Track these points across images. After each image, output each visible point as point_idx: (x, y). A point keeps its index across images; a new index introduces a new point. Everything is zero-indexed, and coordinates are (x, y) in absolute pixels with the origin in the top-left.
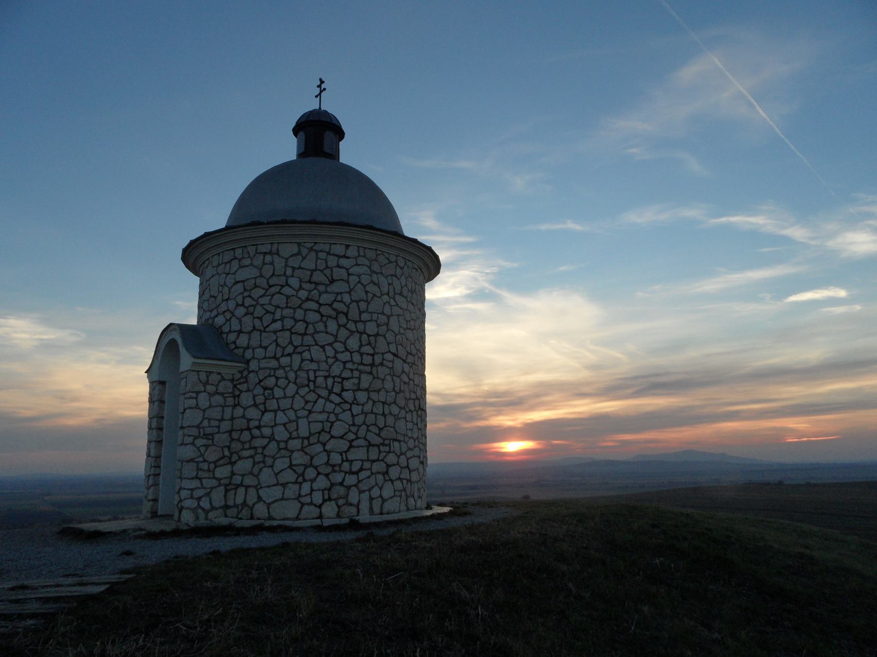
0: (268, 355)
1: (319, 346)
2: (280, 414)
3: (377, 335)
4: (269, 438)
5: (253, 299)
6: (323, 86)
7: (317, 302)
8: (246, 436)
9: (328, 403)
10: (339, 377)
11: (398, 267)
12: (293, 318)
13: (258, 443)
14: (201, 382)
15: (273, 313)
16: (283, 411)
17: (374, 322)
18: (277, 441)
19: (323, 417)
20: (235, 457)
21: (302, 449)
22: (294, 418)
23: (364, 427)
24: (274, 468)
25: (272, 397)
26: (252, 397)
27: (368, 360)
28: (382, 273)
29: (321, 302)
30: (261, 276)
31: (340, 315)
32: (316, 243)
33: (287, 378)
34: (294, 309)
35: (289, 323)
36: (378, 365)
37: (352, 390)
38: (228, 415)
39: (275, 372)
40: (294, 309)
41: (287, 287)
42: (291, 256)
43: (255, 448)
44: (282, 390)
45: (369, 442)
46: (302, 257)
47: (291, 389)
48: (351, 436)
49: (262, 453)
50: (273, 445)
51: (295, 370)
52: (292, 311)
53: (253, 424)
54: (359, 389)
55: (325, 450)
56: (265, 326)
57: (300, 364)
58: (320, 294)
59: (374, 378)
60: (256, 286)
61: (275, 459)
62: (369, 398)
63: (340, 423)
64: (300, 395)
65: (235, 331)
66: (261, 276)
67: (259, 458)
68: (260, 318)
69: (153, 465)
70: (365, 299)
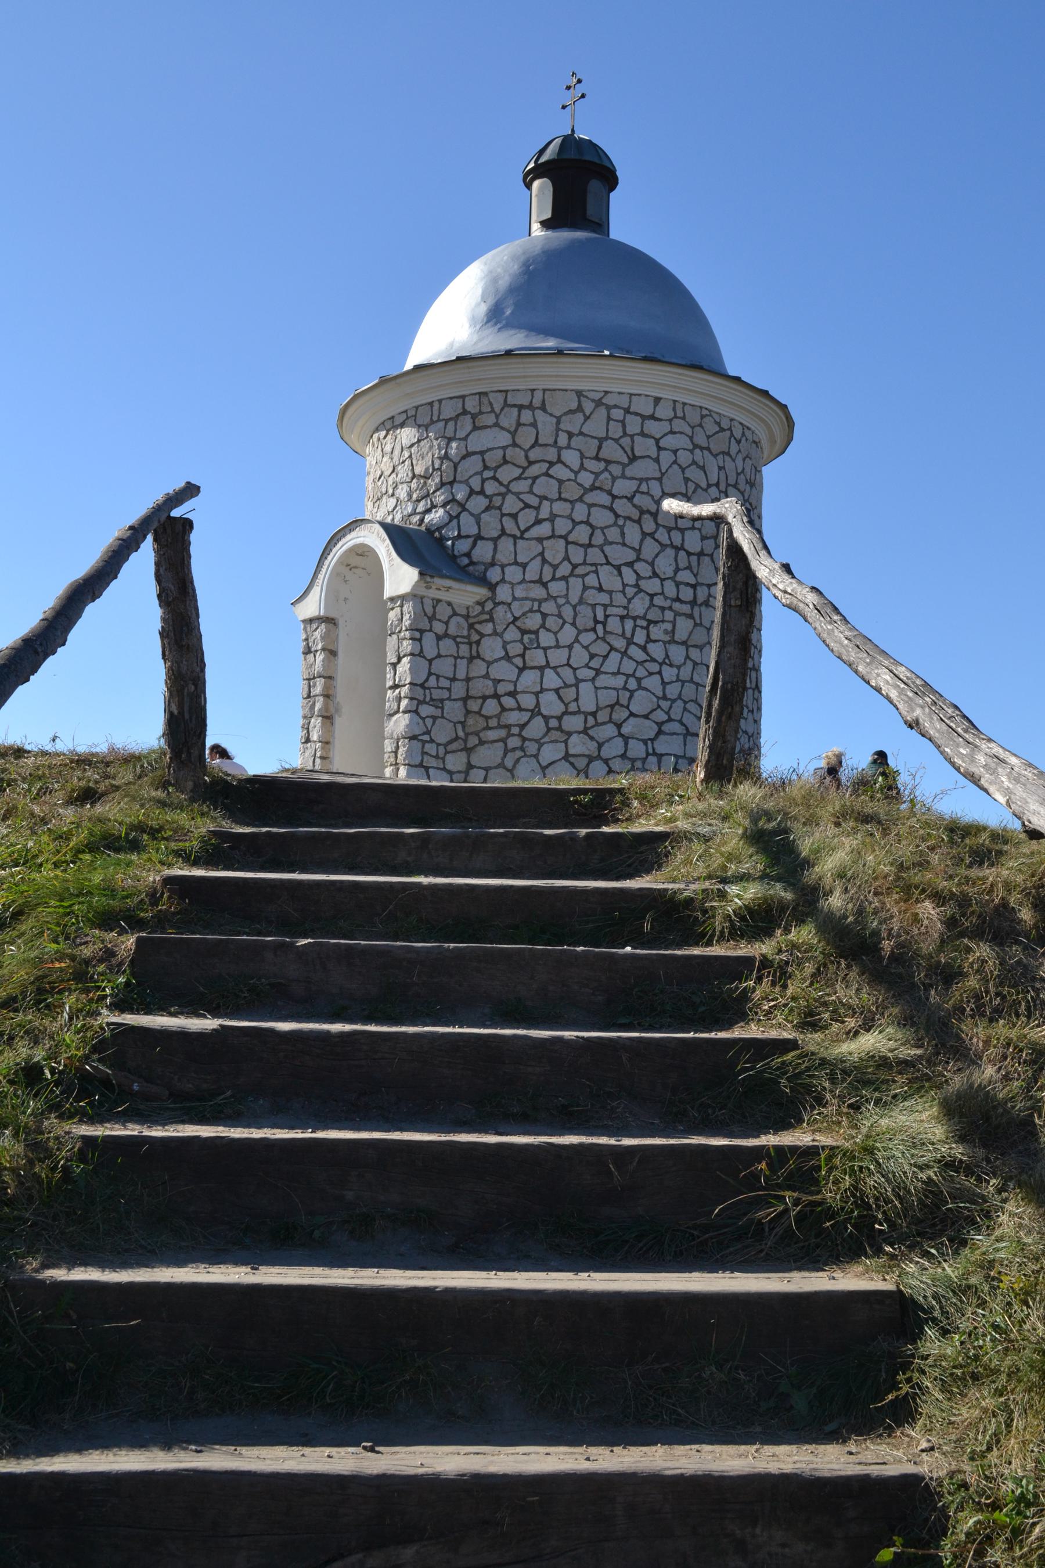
0: (527, 578)
1: (612, 565)
2: (548, 672)
3: (701, 554)
4: (532, 711)
5: (501, 484)
6: (580, 89)
7: (610, 493)
8: (491, 707)
9: (625, 658)
10: (644, 618)
11: (732, 438)
12: (570, 517)
13: (514, 718)
14: (426, 615)
15: (537, 509)
16: (555, 668)
17: (697, 532)
18: (544, 717)
19: (619, 681)
20: (473, 741)
21: (585, 731)
22: (573, 681)
23: (680, 703)
24: (540, 758)
25: (535, 645)
26: (501, 644)
27: (687, 594)
28: (708, 449)
29: (615, 492)
30: (515, 445)
31: (646, 516)
32: (606, 392)
33: (560, 616)
34: (571, 502)
35: (562, 526)
36: (701, 605)
37: (663, 641)
38: (461, 674)
39: (540, 606)
40: (571, 502)
41: (559, 465)
42: (565, 414)
43: (508, 727)
44: (552, 635)
45: (687, 729)
46: (584, 415)
47: (568, 634)
48: (660, 716)
49: (520, 735)
50: (538, 723)
51: (573, 604)
52: (568, 505)
53: (502, 689)
54: (673, 641)
55: (620, 735)
56: (522, 528)
57: (582, 595)
58: (614, 479)
59: (696, 625)
60: (505, 462)
61: (541, 745)
62: (687, 657)
63: (644, 693)
64: (581, 644)
65: (468, 537)
66: (515, 445)
67: (514, 742)
68: (514, 516)
69: (318, 754)
70: (684, 492)
